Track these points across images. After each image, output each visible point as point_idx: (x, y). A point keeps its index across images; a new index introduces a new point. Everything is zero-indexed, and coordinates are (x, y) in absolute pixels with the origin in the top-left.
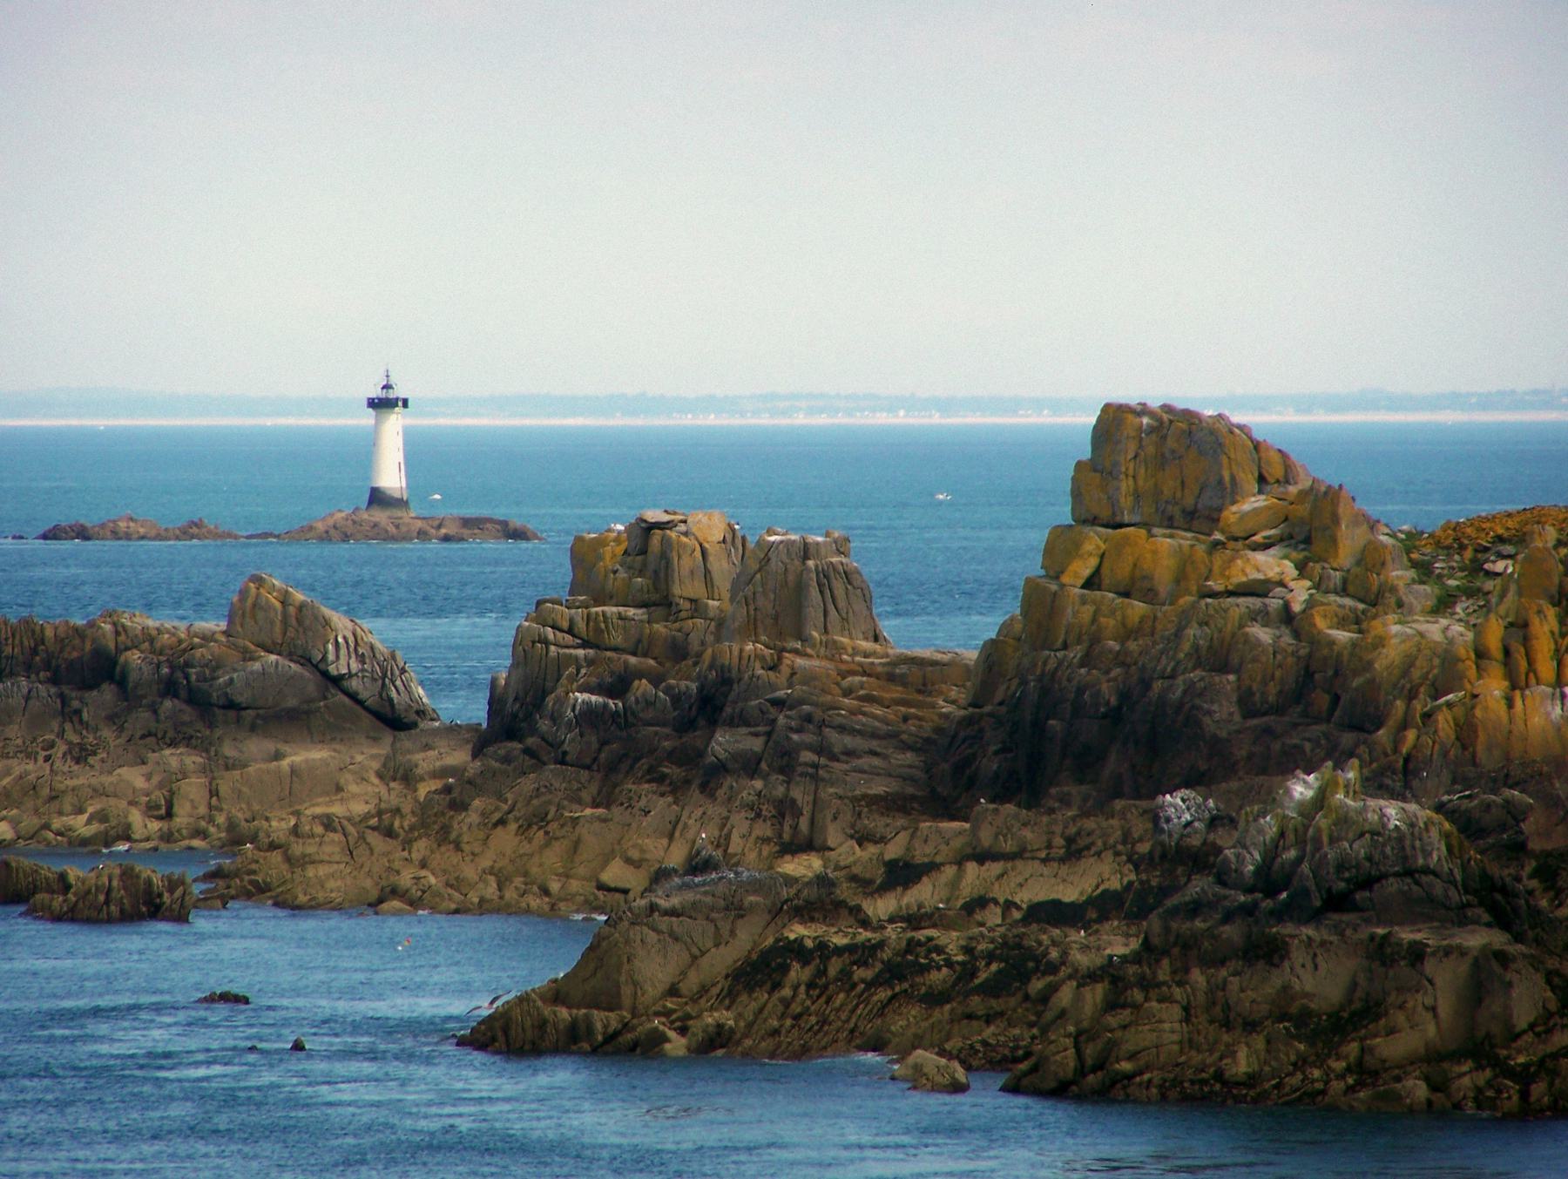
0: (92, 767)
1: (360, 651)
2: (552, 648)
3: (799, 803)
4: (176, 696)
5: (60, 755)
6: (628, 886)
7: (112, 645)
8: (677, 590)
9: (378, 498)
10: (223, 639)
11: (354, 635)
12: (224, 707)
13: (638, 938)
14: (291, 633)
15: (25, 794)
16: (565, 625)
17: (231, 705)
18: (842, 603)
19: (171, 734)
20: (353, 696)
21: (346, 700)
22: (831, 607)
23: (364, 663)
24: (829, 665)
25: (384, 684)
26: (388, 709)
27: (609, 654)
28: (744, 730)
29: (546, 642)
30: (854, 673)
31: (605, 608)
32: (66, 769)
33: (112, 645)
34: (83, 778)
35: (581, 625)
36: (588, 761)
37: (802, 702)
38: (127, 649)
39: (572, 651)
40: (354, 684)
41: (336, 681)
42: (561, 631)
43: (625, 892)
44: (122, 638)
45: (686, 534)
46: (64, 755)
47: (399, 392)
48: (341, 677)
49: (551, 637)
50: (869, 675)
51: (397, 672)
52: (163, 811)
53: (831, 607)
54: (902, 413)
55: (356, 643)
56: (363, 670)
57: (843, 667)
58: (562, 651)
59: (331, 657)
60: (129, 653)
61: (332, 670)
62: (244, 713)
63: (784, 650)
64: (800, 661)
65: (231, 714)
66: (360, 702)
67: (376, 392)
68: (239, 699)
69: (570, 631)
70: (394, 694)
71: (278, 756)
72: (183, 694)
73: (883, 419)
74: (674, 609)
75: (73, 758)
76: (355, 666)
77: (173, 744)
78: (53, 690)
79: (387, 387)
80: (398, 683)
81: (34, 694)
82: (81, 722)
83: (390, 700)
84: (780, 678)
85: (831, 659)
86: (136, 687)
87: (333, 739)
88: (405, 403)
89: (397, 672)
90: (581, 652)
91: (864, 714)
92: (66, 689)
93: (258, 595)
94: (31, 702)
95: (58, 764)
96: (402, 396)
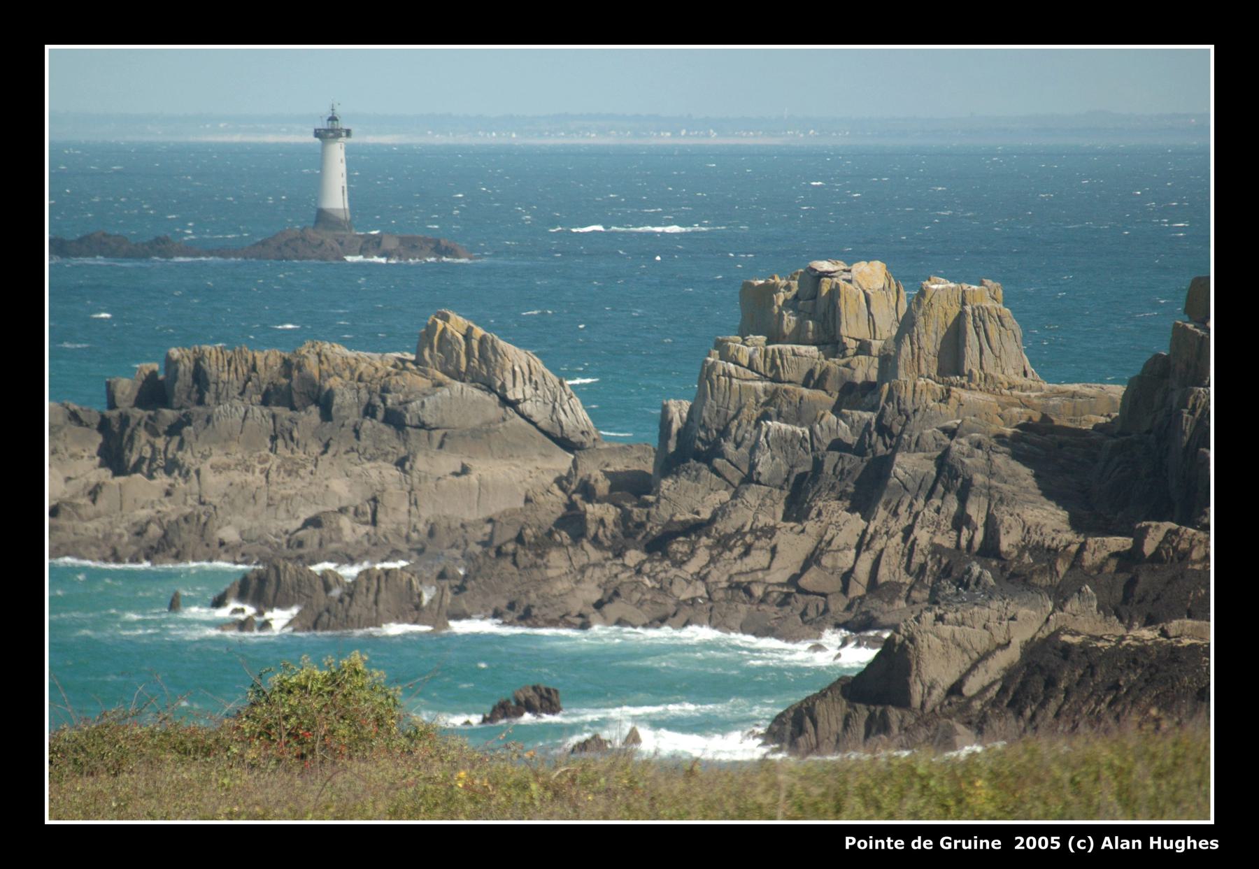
0: (302, 478)
1: (534, 379)
2: (734, 381)
3: (974, 518)
4: (373, 416)
5: (274, 468)
6: (826, 591)
7: (316, 373)
8: (844, 331)
9: (323, 218)
10: (414, 367)
12: (416, 427)
16: (745, 362)
18: (995, 344)
19: (371, 450)
20: (528, 419)
21: (522, 421)
22: (985, 346)
23: (536, 389)
24: (991, 398)
25: (554, 407)
26: (558, 429)
27: (787, 386)
30: (1014, 405)
31: (780, 346)
32: (280, 480)
33: (316, 373)
34: (293, 486)
36: (779, 482)
37: (971, 431)
38: (330, 376)
39: (750, 383)
40: (527, 407)
41: (514, 404)
43: (824, 595)
44: (325, 366)
45: (850, 281)
46: (278, 467)
48: (518, 401)
49: (733, 372)
50: (1026, 407)
51: (565, 398)
53: (985, 346)
55: (531, 373)
56: (536, 395)
57: (1003, 399)
59: (509, 385)
60: (332, 380)
62: (433, 432)
63: (952, 384)
64: (966, 395)
65: (423, 432)
67: (324, 125)
68: (428, 420)
69: (750, 367)
70: (563, 417)
71: (465, 470)
73: (666, 139)
75: (285, 471)
76: (529, 390)
77: (372, 459)
78: (266, 411)
79: (333, 119)
80: (567, 407)
81: (250, 415)
82: (292, 439)
83: (560, 422)
87: (511, 456)
88: (348, 133)
89: (565, 398)
92: (277, 410)
93: (444, 330)
94: (248, 422)
95: (273, 475)
96: (346, 127)
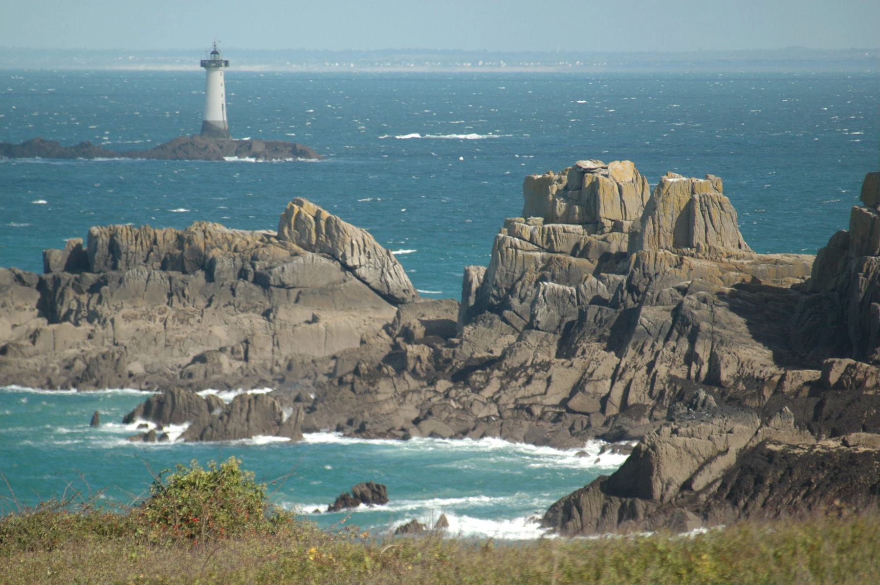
0: (192, 325)
1: (367, 250)
4: (246, 278)
5: (170, 317)
6: (589, 411)
9: (207, 128)
11: (364, 240)
12: (278, 287)
13: (664, 452)
14: (323, 238)
15: (150, 343)
16: (528, 237)
17: (283, 285)
18: (717, 223)
19: (244, 304)
20: (363, 280)
22: (710, 225)
23: (369, 258)
25: (382, 272)
26: (386, 288)
27: (559, 255)
28: (661, 307)
29: (516, 248)
30: (731, 270)
31: (554, 225)
32: (175, 327)
34: (185, 331)
35: (538, 237)
38: (212, 248)
39: (531, 253)
40: (362, 272)
41: (352, 269)
42: (525, 240)
44: (209, 241)
45: (607, 176)
46: (174, 317)
47: (223, 57)
48: (355, 267)
49: (518, 245)
50: (741, 271)
52: (242, 355)
53: (710, 225)
54: (480, 63)
55: (365, 246)
57: (723, 265)
58: (525, 253)
59: (348, 254)
61: (349, 263)
62: (291, 290)
63: (684, 254)
65: (283, 290)
66: (368, 284)
67: (208, 57)
68: (287, 281)
69: (531, 241)
70: (389, 279)
72: (251, 277)
73: (467, 68)
74: (599, 225)
75: (179, 320)
76: (363, 259)
77: (244, 310)
78: (164, 274)
79: (215, 53)
80: (392, 271)
81: (152, 277)
82: (184, 295)
83: (387, 282)
84: (682, 273)
85: (715, 260)
86: (219, 274)
88: (227, 63)
89: (391, 264)
90: (538, 255)
91: (740, 297)
92: (173, 273)
94: (151, 283)
96: (224, 59)
